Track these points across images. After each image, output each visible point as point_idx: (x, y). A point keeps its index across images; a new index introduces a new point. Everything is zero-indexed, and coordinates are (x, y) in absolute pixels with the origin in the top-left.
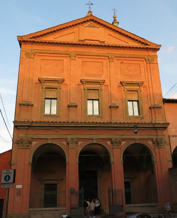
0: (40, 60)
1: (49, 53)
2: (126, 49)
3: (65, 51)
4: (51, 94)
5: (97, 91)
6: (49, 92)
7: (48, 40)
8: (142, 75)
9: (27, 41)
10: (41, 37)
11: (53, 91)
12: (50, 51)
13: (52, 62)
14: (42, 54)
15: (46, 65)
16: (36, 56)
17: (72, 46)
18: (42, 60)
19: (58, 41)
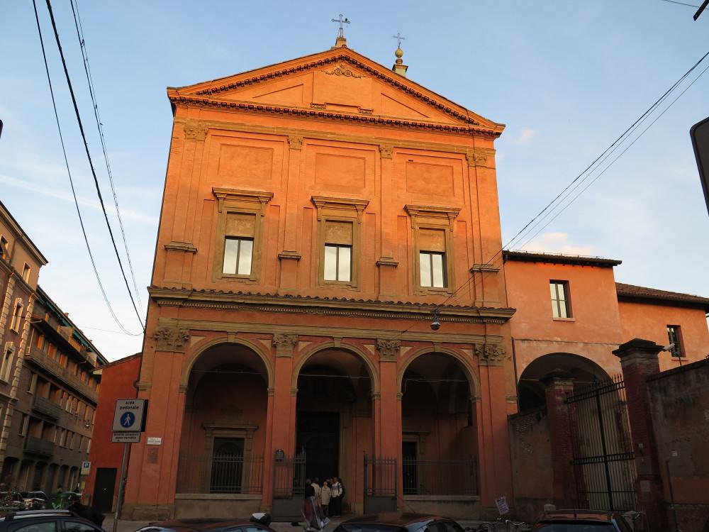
4: (241, 228)
6: (236, 222)
9: (191, 101)
13: (245, 151)
15: (232, 158)
16: (209, 136)
18: (224, 148)
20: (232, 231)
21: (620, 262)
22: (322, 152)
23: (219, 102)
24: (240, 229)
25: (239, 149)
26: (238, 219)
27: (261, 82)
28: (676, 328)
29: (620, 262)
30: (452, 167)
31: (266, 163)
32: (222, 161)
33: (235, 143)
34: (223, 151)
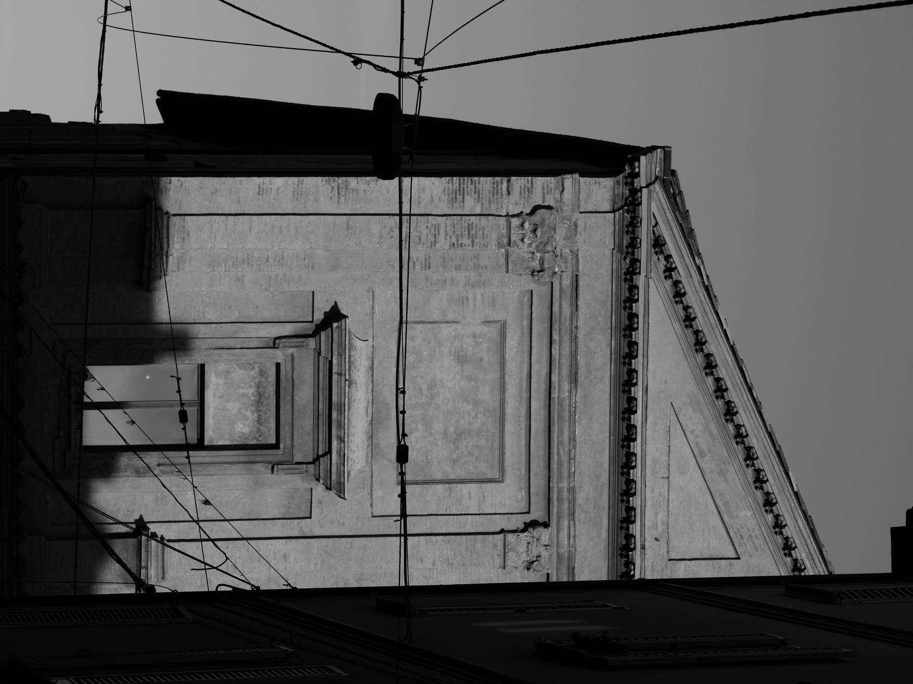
0: (500, 316)
1: (555, 378)
2: (619, 287)
3: (572, 490)
4: (234, 407)
5: (375, 515)
6: (251, 391)
7: (646, 366)
8: (509, 563)
9: (633, 224)
10: (692, 339)
11: (259, 420)
12: (566, 386)
13: (486, 394)
14: (539, 327)
15: (461, 359)
16: (528, 283)
17: (619, 320)
18: (494, 330)
19: (646, 356)
20: (221, 382)
21: (427, 80)
22: (512, 343)
23: (640, 281)
24: (229, 405)
25: (493, 376)
26: (260, 395)
27: (700, 358)
28: (261, 415)
29: (427, 80)
30: (500, 481)
31: (455, 462)
32: (446, 331)
33: (512, 366)
34: (478, 329)
